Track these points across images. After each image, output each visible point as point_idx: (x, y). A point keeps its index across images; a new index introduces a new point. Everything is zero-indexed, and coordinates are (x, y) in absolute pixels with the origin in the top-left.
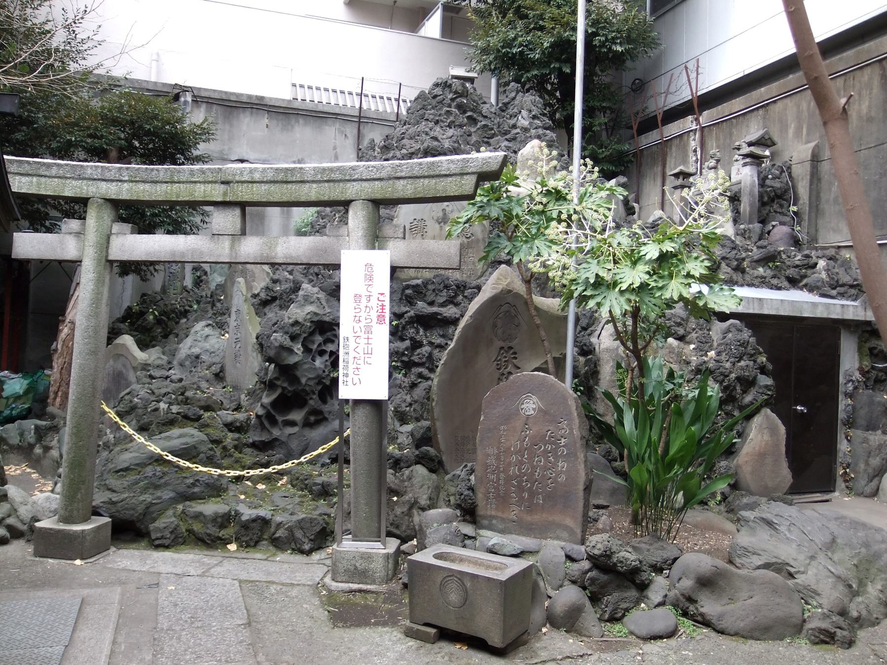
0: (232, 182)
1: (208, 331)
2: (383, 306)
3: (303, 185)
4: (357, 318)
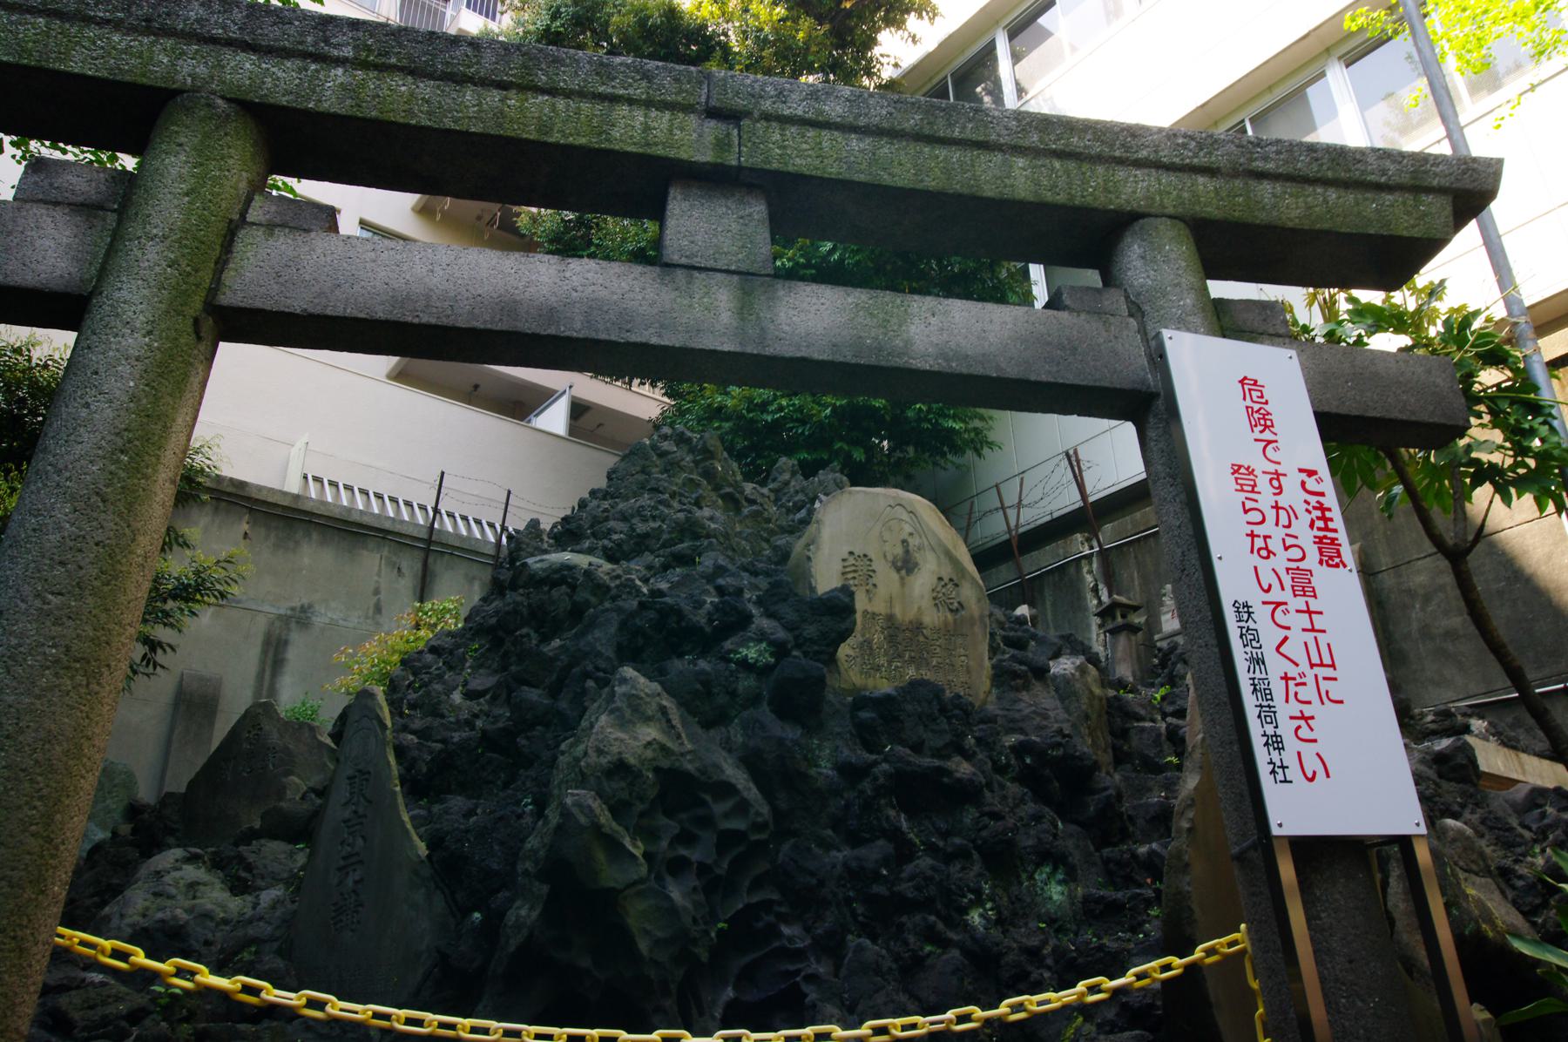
0: (748, 114)
1: (191, 872)
2: (1321, 507)
3: (984, 157)
4: (1259, 543)
